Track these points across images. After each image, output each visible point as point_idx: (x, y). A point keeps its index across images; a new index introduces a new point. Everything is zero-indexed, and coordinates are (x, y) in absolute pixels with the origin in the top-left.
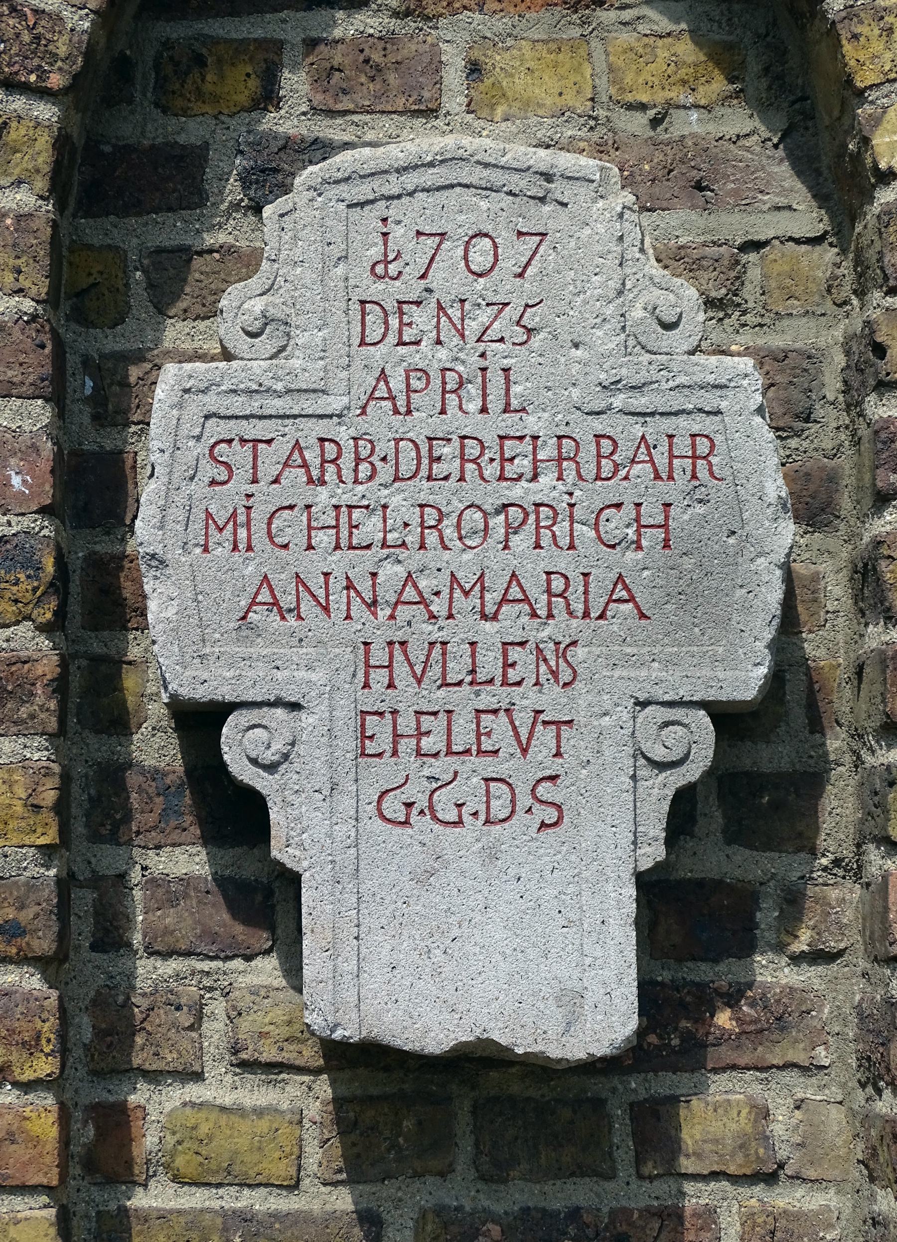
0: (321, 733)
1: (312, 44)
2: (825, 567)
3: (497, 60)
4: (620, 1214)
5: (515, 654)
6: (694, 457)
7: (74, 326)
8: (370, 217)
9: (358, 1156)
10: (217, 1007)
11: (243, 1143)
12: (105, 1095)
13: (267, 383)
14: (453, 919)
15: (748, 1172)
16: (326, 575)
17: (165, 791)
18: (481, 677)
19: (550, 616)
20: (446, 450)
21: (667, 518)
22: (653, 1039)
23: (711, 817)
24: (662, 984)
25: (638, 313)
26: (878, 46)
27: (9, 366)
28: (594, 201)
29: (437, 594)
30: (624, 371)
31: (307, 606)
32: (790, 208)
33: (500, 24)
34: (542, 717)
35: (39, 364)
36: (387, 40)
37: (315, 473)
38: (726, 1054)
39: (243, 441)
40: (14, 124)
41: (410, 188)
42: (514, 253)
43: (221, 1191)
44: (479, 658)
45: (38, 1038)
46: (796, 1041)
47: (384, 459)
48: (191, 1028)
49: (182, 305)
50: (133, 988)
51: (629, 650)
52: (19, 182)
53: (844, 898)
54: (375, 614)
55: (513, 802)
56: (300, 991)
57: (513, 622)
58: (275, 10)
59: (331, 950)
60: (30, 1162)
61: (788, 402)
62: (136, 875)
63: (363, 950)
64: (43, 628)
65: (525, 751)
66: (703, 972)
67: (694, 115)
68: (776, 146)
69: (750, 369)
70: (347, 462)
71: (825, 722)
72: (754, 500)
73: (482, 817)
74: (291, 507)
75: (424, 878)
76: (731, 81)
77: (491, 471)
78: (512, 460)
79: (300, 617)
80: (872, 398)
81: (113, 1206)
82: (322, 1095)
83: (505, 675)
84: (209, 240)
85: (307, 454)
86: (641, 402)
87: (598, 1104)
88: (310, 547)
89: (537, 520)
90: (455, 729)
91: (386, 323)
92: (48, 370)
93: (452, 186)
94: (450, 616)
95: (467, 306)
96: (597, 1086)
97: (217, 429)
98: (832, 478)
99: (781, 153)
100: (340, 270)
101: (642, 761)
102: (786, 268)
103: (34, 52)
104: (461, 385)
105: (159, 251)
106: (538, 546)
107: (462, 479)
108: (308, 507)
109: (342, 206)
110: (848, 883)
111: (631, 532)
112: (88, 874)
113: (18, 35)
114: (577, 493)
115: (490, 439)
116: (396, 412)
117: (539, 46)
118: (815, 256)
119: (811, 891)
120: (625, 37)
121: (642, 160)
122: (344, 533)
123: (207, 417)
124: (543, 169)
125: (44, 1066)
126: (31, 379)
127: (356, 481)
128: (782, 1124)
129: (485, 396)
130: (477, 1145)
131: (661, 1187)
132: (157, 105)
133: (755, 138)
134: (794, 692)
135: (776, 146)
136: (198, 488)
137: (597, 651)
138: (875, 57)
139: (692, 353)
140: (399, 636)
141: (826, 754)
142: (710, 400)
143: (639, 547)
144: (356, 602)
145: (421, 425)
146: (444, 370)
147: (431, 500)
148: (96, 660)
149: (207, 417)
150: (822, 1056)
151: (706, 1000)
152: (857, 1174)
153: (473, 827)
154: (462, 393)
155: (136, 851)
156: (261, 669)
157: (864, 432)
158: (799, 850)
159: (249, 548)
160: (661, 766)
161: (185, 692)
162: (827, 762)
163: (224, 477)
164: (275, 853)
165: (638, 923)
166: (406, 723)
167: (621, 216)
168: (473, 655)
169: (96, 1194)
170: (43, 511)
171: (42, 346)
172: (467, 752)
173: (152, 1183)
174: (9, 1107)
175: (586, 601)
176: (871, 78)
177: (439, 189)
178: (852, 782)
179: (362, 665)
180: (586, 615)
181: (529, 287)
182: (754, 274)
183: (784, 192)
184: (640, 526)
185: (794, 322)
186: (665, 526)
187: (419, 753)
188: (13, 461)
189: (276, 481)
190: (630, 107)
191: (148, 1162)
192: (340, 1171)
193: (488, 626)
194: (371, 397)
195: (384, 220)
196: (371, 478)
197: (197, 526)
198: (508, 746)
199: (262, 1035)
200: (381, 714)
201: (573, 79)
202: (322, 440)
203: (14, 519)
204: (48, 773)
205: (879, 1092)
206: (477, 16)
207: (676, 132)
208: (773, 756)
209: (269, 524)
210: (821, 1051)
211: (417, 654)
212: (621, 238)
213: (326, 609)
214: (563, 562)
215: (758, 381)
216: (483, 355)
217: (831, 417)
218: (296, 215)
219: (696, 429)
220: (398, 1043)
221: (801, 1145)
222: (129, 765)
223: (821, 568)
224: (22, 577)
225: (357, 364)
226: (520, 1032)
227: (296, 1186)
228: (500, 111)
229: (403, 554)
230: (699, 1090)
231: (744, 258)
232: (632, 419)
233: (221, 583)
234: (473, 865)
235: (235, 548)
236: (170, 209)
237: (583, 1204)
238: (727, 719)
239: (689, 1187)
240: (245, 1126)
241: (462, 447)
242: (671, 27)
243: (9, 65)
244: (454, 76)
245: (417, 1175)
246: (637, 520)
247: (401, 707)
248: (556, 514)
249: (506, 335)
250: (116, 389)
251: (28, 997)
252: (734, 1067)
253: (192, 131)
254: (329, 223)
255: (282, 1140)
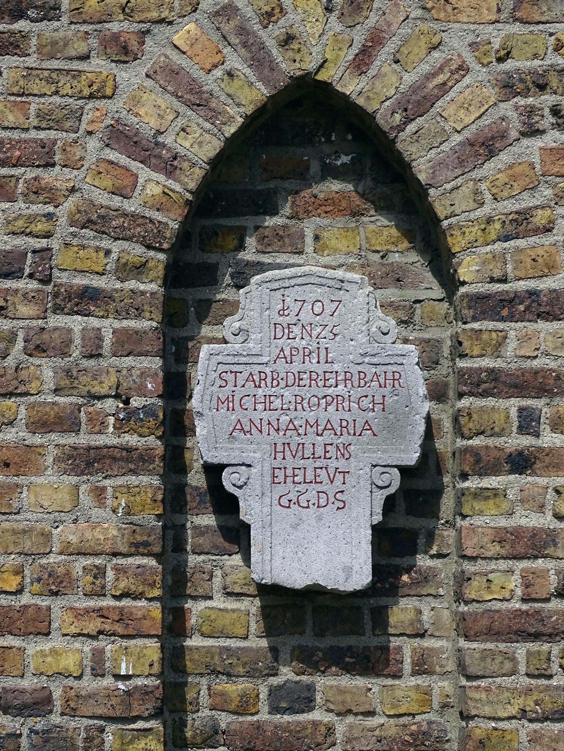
0: (258, 475)
1: (257, 228)
2: (443, 416)
3: (325, 234)
4: (367, 648)
5: (329, 448)
6: (394, 380)
7: (168, 327)
8: (278, 294)
9: (270, 627)
10: (218, 573)
11: (227, 622)
12: (176, 604)
13: (240, 352)
14: (305, 541)
15: (414, 633)
16: (261, 419)
17: (200, 495)
18: (316, 456)
19: (342, 435)
20: (305, 376)
21: (384, 401)
22: (379, 585)
23: (401, 505)
24: (383, 565)
25: (374, 329)
26: (460, 238)
27: (147, 345)
28: (359, 290)
29: (301, 426)
30: (369, 350)
31: (254, 430)
32: (431, 288)
33: (326, 221)
34: (338, 470)
35: (158, 345)
36: (285, 227)
37: (257, 384)
38: (406, 591)
39: (231, 372)
40: (150, 261)
41: (293, 284)
42: (330, 308)
43: (219, 640)
44: (316, 449)
45: (155, 582)
46: (432, 586)
47: (282, 379)
48: (208, 580)
49: (208, 320)
50: (187, 565)
51: (370, 447)
52: (152, 281)
53: (449, 534)
54: (278, 433)
55: (328, 500)
56: (250, 567)
57: (328, 437)
58: (244, 215)
59: (262, 552)
60: (151, 626)
61: (430, 357)
62: (189, 525)
63: (273, 552)
64: (158, 438)
65: (332, 482)
66: (397, 561)
67: (397, 255)
68: (427, 266)
69: (414, 349)
70: (269, 380)
71: (443, 472)
72: (415, 395)
73: (316, 505)
74: (248, 396)
75: (295, 527)
76: (410, 243)
77: (321, 384)
78: (328, 380)
79: (251, 434)
80: (458, 359)
81: (179, 645)
82: (257, 605)
83: (325, 455)
84: (218, 297)
85: (254, 377)
86: (375, 360)
87: (359, 608)
88: (255, 410)
89: (337, 401)
90: (307, 474)
91: (283, 331)
92: (161, 347)
93: (308, 284)
94: (306, 434)
95: (313, 326)
96: (358, 602)
97: (222, 368)
98: (446, 385)
99: (428, 269)
100: (267, 313)
101: (374, 486)
102: (430, 310)
103: (158, 236)
104: (310, 353)
105: (200, 300)
106: (337, 410)
107: (310, 386)
108: (255, 395)
109: (268, 290)
110: (451, 529)
111: (371, 405)
112: (171, 524)
113: (152, 230)
114: (352, 392)
115: (320, 372)
116: (287, 362)
117: (340, 230)
118: (441, 305)
119: (437, 532)
120: (372, 227)
121: (377, 270)
122: (268, 405)
123: (218, 364)
124: (340, 278)
125: (157, 592)
126: (155, 350)
127: (272, 387)
128: (426, 616)
129: (319, 357)
130: (314, 623)
131: (382, 639)
132: (200, 249)
133: (419, 263)
134: (431, 462)
135: (427, 266)
136: (215, 389)
137: (358, 447)
138: (459, 242)
139: (394, 343)
140: (287, 441)
141: (443, 483)
142: (400, 360)
143: (374, 411)
144: (272, 431)
145: (296, 367)
146: (304, 348)
147: (299, 393)
148: (175, 447)
149: (218, 364)
150: (441, 591)
151: (398, 571)
152: (454, 634)
153: (313, 509)
154: (311, 356)
155: (189, 516)
156: (237, 453)
157: (456, 370)
158: (433, 517)
159: (233, 410)
160: (381, 488)
161: (209, 460)
162: (444, 486)
163: (224, 385)
164: (241, 517)
165: (373, 543)
166: (289, 472)
167: (368, 295)
168: (314, 448)
169: (172, 640)
170: (159, 396)
171: (160, 339)
172: (311, 482)
173: (193, 637)
174: (144, 607)
175: (354, 430)
176: (458, 250)
177: (303, 285)
178: (453, 493)
179: (273, 451)
180: (354, 434)
181: (335, 319)
182: (418, 312)
183: (430, 283)
184: (374, 404)
185: (433, 329)
186: (383, 404)
187: (294, 482)
188: (148, 379)
189: (243, 386)
190: (374, 252)
191: (192, 629)
192: (263, 632)
193: (319, 438)
194: (278, 357)
195: (283, 295)
196: (277, 386)
197: (214, 402)
198: (326, 480)
199: (235, 583)
200: (280, 469)
201: (353, 241)
202: (260, 372)
203: (148, 399)
204: (159, 488)
205: (460, 603)
206: (318, 219)
207: (390, 261)
208: (424, 484)
209: (241, 401)
210: (441, 590)
211: (294, 447)
212: (368, 303)
213: (261, 432)
214: (346, 416)
215: (417, 353)
216: (318, 343)
217: (446, 363)
218: (251, 293)
219: (394, 370)
220: (285, 585)
221: (433, 624)
222: (186, 485)
223: (442, 417)
224: (151, 420)
225: (273, 345)
226: (329, 581)
227: (247, 638)
228: (326, 253)
229: (289, 412)
230: (396, 603)
231: (415, 306)
232: (372, 366)
233: (223, 422)
234: (313, 522)
235: (228, 410)
236: (204, 286)
237: (353, 645)
238: (404, 470)
239: (392, 639)
240: (228, 616)
241: (311, 375)
242: (389, 223)
243: (149, 240)
244: (309, 240)
245: (292, 634)
246: (373, 401)
247: (287, 466)
248: (344, 399)
249: (327, 336)
250: (183, 350)
251: (151, 568)
252: (409, 595)
253: (212, 258)
254: (263, 296)
255: (242, 621)
